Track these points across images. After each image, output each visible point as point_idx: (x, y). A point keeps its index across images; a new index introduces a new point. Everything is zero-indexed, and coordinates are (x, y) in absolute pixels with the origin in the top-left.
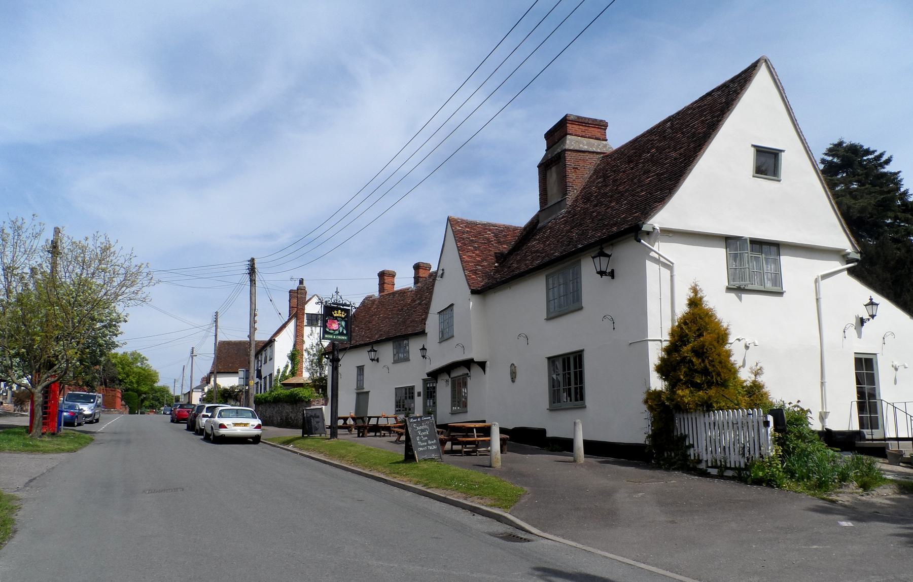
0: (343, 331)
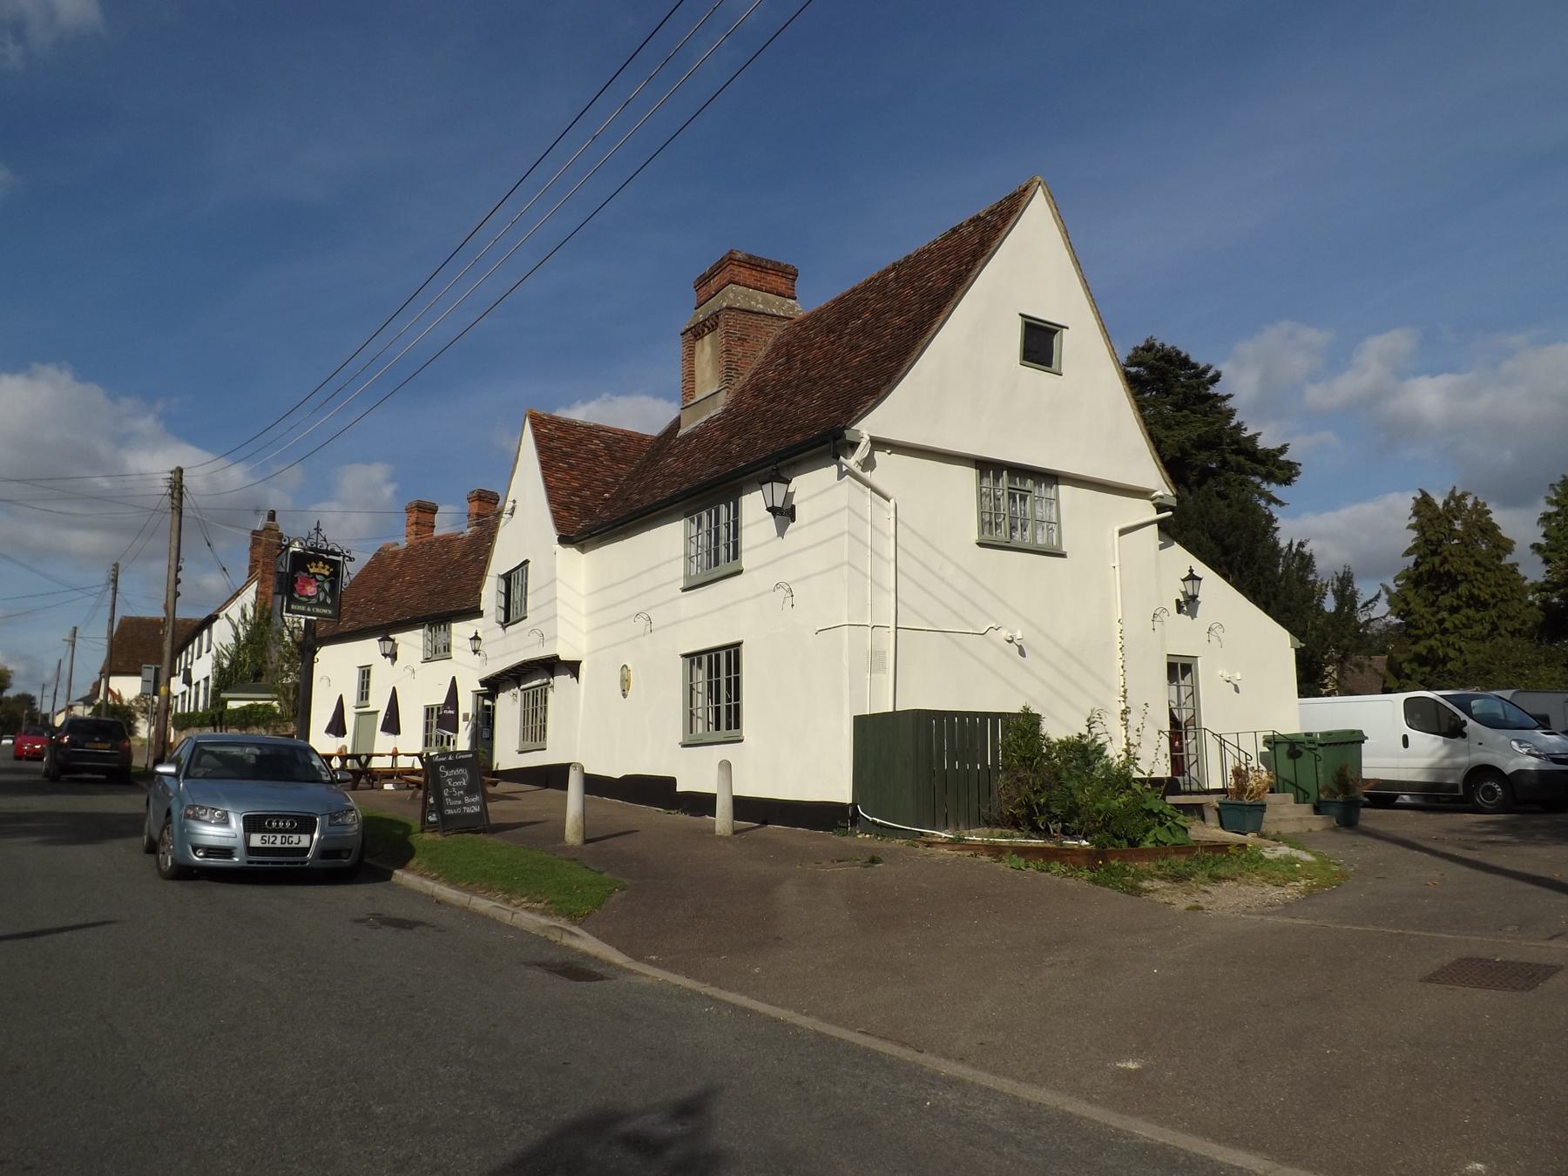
0: (325, 598)
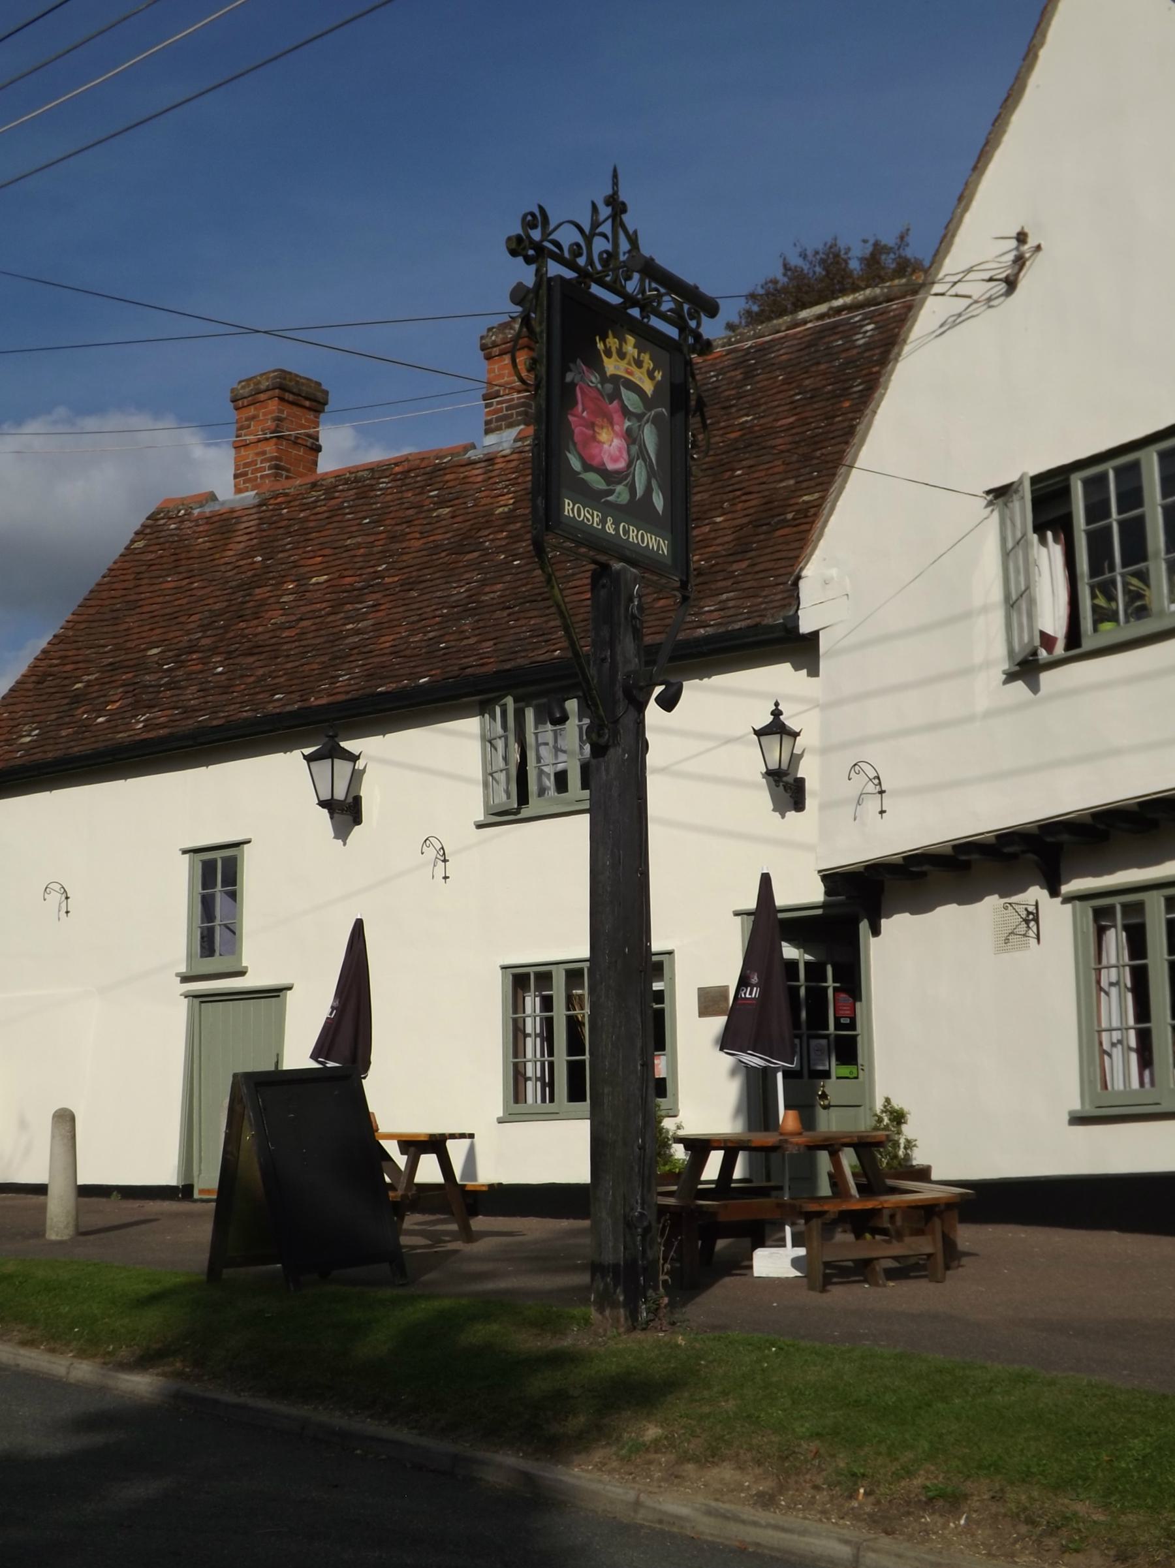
0: (648, 490)
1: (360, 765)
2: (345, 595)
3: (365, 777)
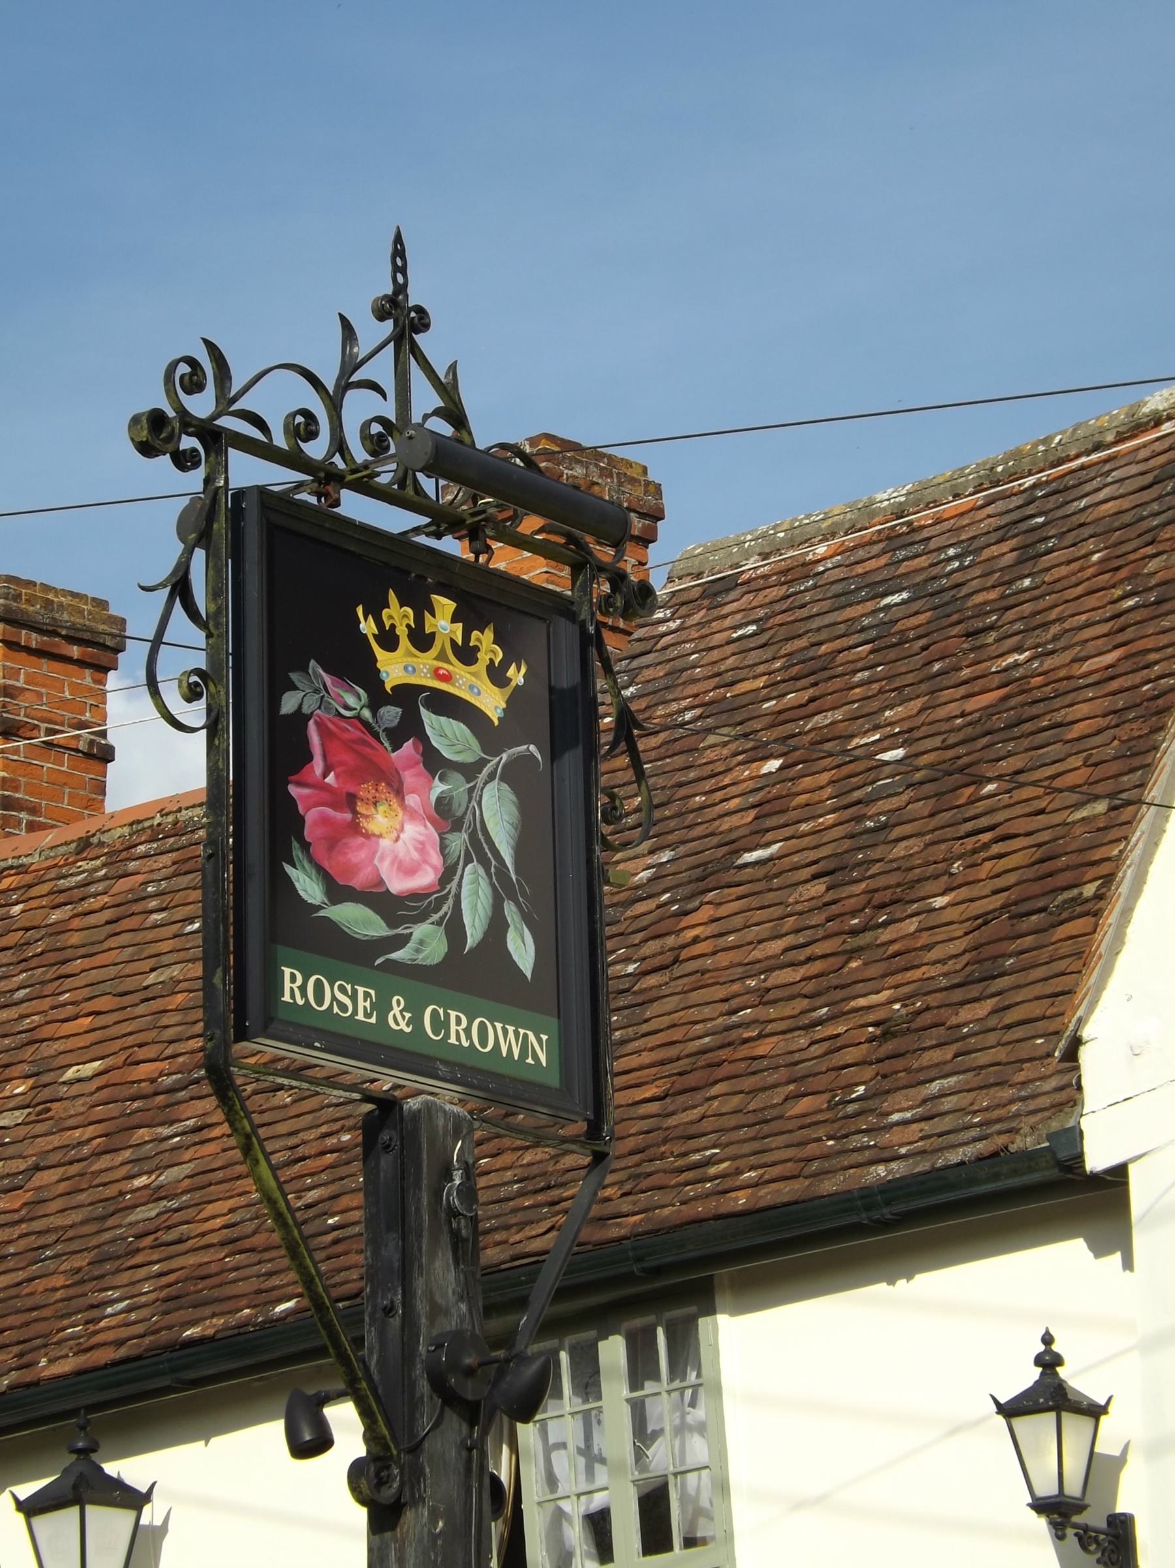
0: (497, 927)
1: (151, 1515)
2: (136, 1105)
3: (168, 1545)
